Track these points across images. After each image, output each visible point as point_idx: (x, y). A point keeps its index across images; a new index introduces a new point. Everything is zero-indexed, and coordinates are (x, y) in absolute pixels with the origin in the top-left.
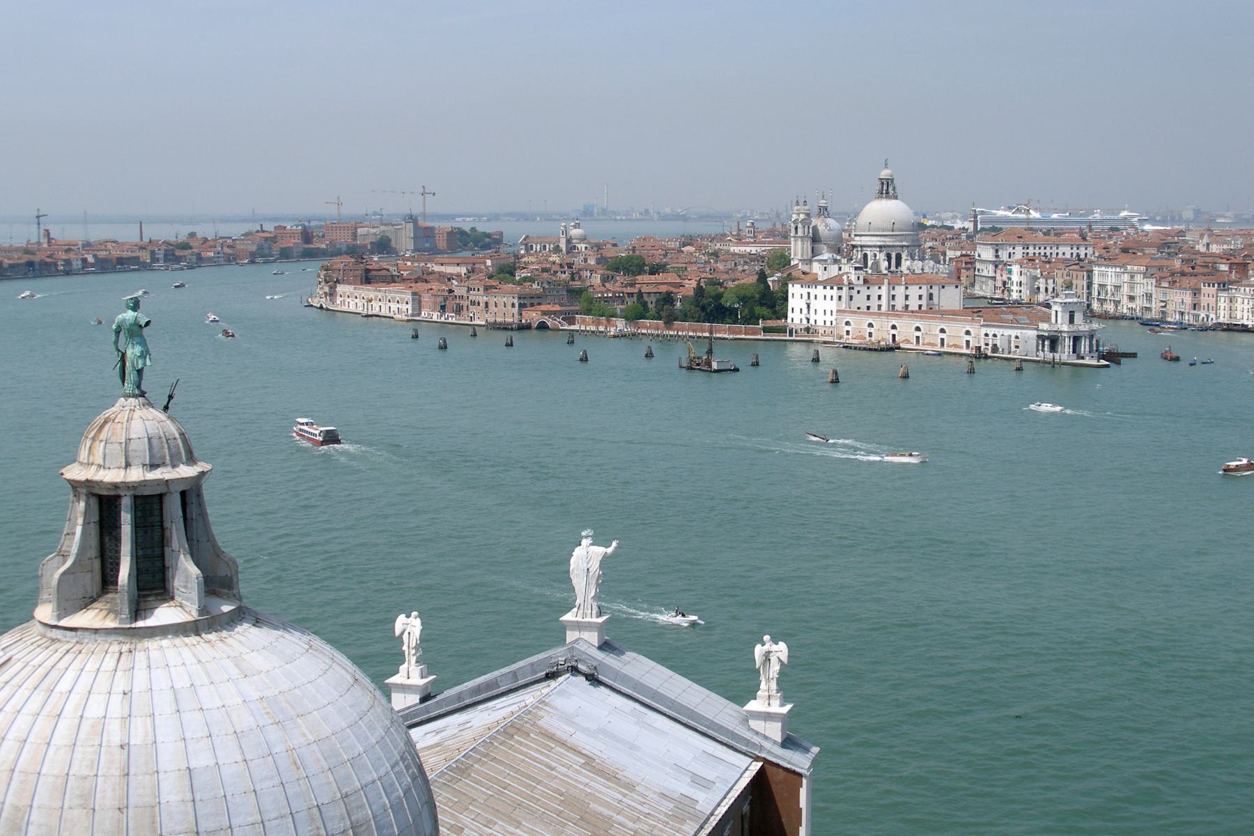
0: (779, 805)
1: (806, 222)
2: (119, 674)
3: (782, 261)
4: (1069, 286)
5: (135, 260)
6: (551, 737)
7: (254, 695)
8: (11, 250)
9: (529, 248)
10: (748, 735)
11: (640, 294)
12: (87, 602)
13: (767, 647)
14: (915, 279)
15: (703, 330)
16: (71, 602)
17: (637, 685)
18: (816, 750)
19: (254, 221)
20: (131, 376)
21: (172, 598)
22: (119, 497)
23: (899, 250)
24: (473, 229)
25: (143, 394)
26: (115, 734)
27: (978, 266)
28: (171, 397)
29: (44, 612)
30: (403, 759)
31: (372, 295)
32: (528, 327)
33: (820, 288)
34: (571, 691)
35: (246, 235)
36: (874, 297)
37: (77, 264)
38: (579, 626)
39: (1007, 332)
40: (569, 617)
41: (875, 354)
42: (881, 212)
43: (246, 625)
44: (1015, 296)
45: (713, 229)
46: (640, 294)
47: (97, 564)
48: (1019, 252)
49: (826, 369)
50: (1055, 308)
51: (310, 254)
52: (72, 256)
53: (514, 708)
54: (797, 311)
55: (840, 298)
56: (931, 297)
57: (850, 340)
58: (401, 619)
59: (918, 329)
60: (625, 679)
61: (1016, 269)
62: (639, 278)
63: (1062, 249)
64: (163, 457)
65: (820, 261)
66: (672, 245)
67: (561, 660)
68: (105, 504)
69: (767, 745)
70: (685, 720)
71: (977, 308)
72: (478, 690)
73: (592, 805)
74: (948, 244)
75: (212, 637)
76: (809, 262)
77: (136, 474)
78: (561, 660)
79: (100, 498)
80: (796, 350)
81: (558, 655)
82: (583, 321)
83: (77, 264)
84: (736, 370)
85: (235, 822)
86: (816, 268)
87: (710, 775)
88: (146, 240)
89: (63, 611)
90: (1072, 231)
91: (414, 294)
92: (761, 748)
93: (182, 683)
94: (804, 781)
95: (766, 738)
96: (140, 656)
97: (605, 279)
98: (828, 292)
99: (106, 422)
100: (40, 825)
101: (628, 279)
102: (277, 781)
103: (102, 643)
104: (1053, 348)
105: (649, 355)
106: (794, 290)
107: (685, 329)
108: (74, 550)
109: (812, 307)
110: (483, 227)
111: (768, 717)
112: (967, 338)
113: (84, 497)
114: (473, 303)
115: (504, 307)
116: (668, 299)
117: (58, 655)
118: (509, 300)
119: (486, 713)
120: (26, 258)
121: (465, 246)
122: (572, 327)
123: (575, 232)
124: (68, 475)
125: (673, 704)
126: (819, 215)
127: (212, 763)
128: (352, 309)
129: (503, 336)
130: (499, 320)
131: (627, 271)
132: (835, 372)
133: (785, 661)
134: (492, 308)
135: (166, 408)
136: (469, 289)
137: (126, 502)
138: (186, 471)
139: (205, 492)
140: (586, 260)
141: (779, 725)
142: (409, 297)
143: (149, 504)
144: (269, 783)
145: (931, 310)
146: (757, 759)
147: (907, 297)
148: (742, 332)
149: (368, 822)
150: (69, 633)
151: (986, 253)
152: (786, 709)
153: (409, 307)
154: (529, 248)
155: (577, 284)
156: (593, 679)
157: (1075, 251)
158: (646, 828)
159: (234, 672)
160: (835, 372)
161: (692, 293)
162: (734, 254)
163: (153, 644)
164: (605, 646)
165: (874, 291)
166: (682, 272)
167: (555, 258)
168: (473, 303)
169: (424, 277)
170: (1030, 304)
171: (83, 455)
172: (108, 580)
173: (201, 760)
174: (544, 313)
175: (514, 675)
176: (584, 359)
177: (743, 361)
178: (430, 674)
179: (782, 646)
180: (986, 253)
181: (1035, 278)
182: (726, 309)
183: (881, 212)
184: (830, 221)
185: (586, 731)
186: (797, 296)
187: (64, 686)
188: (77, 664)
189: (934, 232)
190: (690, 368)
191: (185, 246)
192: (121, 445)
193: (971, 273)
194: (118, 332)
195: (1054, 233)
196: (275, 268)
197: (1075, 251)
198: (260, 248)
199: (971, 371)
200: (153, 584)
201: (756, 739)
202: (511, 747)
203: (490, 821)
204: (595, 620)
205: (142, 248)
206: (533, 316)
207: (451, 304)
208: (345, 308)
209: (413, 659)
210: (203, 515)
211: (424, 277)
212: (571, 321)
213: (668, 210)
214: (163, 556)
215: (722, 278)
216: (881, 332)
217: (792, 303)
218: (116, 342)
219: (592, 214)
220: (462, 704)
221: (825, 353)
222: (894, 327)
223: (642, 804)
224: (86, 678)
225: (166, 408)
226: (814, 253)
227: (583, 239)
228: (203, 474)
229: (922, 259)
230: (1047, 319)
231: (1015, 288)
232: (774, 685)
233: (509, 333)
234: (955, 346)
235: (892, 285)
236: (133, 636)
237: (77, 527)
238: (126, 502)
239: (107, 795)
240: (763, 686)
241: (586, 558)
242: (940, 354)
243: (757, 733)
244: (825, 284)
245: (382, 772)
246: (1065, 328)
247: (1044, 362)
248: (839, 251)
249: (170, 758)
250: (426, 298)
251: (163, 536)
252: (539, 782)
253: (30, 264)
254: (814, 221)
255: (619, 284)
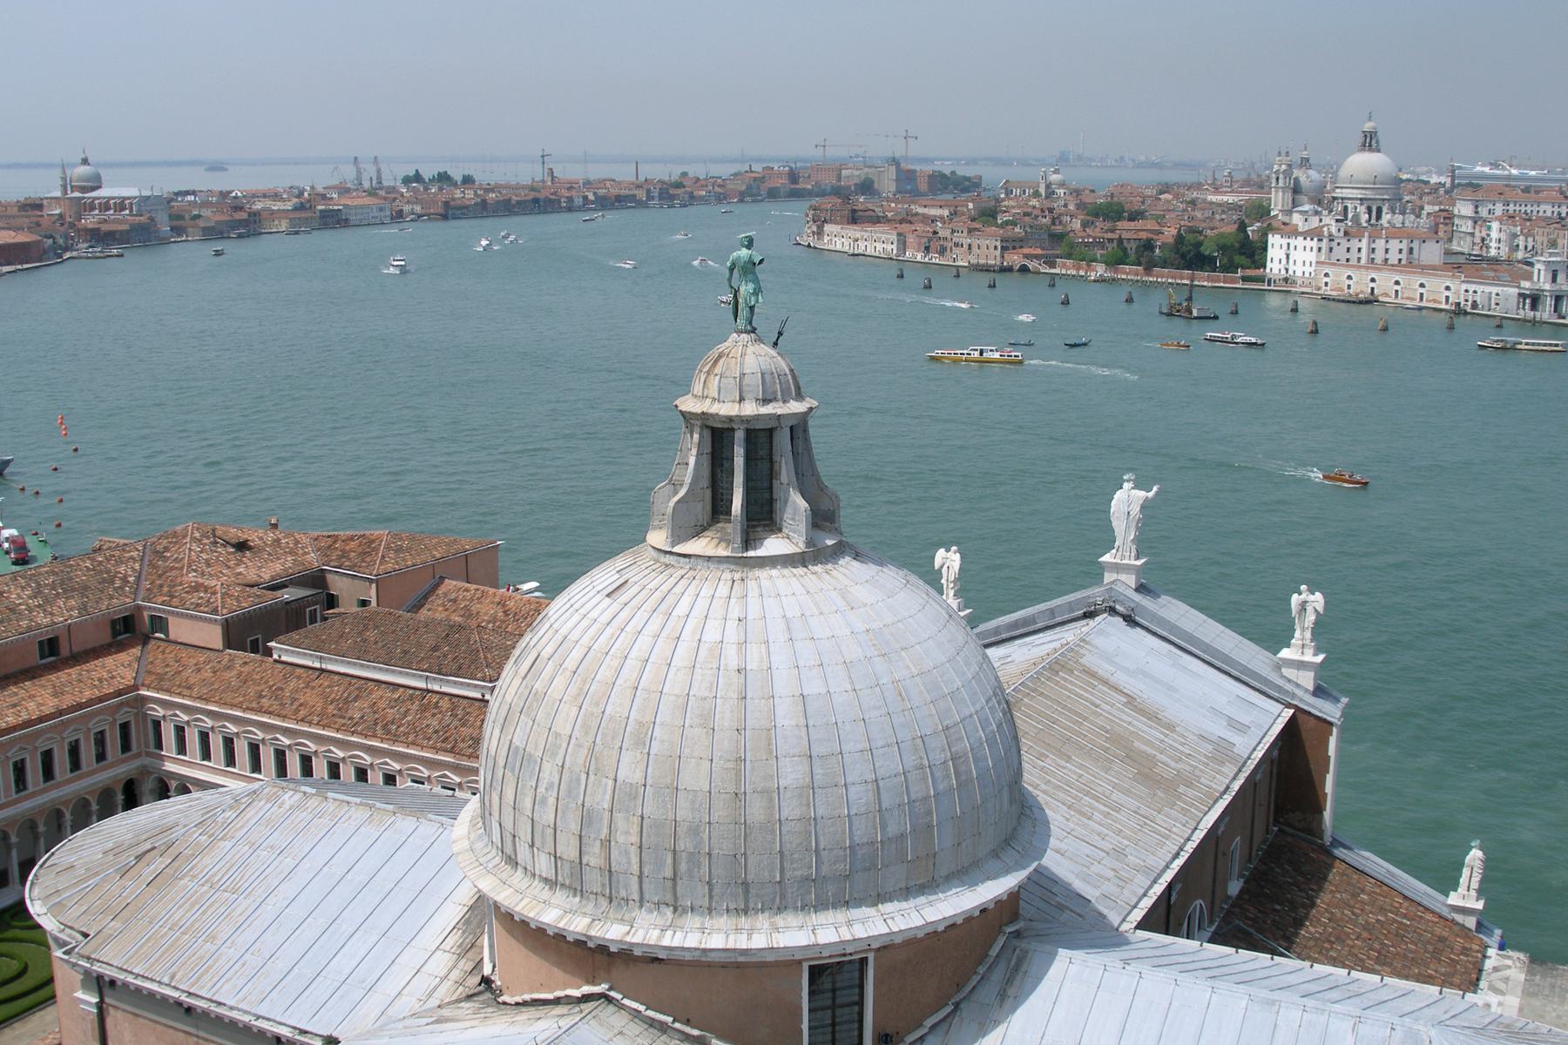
0: (1309, 751)
1: (1288, 173)
2: (733, 601)
3: (1262, 211)
4: (1553, 244)
5: (633, 198)
6: (1093, 675)
7: (861, 627)
8: (518, 187)
9: (1008, 193)
10: (1281, 682)
11: (1120, 240)
12: (698, 531)
13: (1303, 596)
14: (1394, 233)
15: (1184, 278)
16: (685, 529)
17: (1173, 628)
18: (1345, 700)
19: (743, 161)
20: (743, 313)
21: (780, 530)
22: (733, 430)
23: (1380, 203)
24: (953, 173)
25: (754, 331)
26: (731, 659)
27: (1456, 221)
28: (780, 334)
29: (658, 538)
30: (995, 695)
31: (858, 235)
32: (1009, 269)
33: (1300, 239)
34: (1108, 630)
35: (735, 175)
36: (1354, 250)
37: (578, 201)
38: (1117, 568)
39: (1488, 289)
40: (1107, 558)
41: (1354, 307)
42: (1361, 164)
43: (848, 559)
44: (1493, 252)
45: (1190, 178)
46: (1120, 240)
47: (708, 493)
48: (1499, 209)
49: (1305, 319)
50: (1538, 266)
51: (796, 194)
52: (574, 193)
53: (1057, 645)
54: (1276, 261)
55: (1320, 249)
56: (1411, 251)
57: (1328, 291)
58: (941, 553)
59: (1397, 283)
60: (1162, 621)
61: (1495, 225)
62: (1120, 224)
63: (1542, 208)
64: (775, 392)
65: (1301, 212)
66: (1148, 192)
67: (1099, 600)
68: (718, 435)
69: (1299, 692)
70: (1219, 664)
71: (1459, 264)
72: (1015, 625)
73: (1137, 744)
74: (1426, 198)
75: (818, 568)
76: (1289, 213)
77: (750, 409)
78: (1099, 600)
79: (713, 430)
80: (1274, 301)
81: (1095, 593)
82: (1064, 266)
83: (578, 201)
84: (1216, 318)
85: (846, 748)
86: (1297, 219)
87: (1246, 720)
88: (642, 179)
89: (677, 538)
90: (1551, 189)
91: (899, 234)
92: (1294, 696)
93: (793, 612)
94: (1335, 730)
95: (1298, 686)
96: (752, 584)
97: (1085, 225)
98: (1308, 243)
99: (720, 357)
100: (663, 741)
101: (1108, 225)
102: (884, 711)
103: (714, 572)
104: (1534, 307)
105: (1130, 300)
106: (1274, 241)
107: (1163, 276)
108: (688, 480)
109: (1291, 257)
110: (963, 171)
111: (1301, 665)
112: (1447, 293)
113: (697, 429)
114: (956, 245)
115: (986, 249)
116: (1148, 246)
117: (673, 580)
118: (992, 243)
119: (1025, 649)
120: (532, 195)
121: (945, 189)
122: (1057, 271)
123: (1054, 178)
124: (683, 408)
125: (1207, 648)
126: (1301, 166)
127: (824, 691)
128: (839, 247)
129: (986, 278)
130: (982, 262)
131: (1107, 217)
132: (1315, 323)
133: (1321, 609)
134: (975, 250)
135: (776, 344)
136: (953, 231)
137: (739, 435)
138: (796, 407)
139: (811, 431)
140: (1066, 206)
141: (1312, 674)
142: (894, 237)
143: (760, 437)
144: (877, 713)
145: (1410, 264)
146: (1289, 706)
147: (1387, 251)
148: (1220, 281)
149: (966, 754)
150: (682, 560)
151: (1464, 209)
152: (1320, 658)
153: (894, 247)
154: (1008, 193)
155: (1058, 229)
156: (1130, 620)
157: (1556, 209)
158: (1188, 768)
159: (840, 603)
160: (1315, 323)
161: (1171, 240)
162: (1211, 203)
163: (763, 574)
164: (1141, 588)
165: (1355, 244)
166: (1160, 219)
167: (1034, 202)
168: (956, 245)
169: (908, 219)
170: (1509, 261)
171: (697, 388)
172: (719, 509)
173: (813, 688)
174: (1026, 256)
175: (1052, 612)
176: (1066, 302)
177: (1223, 310)
178: (966, 607)
179: (1318, 596)
180: (1464, 209)
181: (1515, 236)
182: (1206, 257)
183: (1361, 164)
184: (1311, 172)
185: (1125, 670)
186: (1276, 246)
187: (681, 609)
188: (692, 590)
189: (1410, 186)
190: (1170, 315)
191: (679, 185)
192: (733, 379)
193: (1449, 228)
194: (732, 270)
195: (1530, 190)
196: (765, 206)
197: (1556, 209)
198: (749, 187)
199: (1451, 327)
200: (763, 516)
201: (1288, 687)
202: (1057, 683)
203: (1042, 755)
204: (1133, 562)
205: (639, 187)
206: (1015, 259)
207: (935, 245)
208: (832, 247)
209: (952, 593)
210: (808, 449)
211: (908, 219)
212: (1052, 265)
213: (1142, 158)
214: (771, 488)
215: (1201, 226)
216: (1360, 284)
217: (1271, 253)
218: (730, 280)
219: (1067, 160)
220: (998, 638)
221: (1303, 304)
222: (1373, 280)
223: (1183, 744)
224: (702, 604)
225: (776, 344)
226: (1295, 204)
227: (1062, 185)
228: (811, 409)
229: (1403, 213)
230: (1529, 277)
231: (1493, 244)
232: (1308, 635)
233: (992, 275)
234: (1434, 301)
235: (1372, 239)
236: (745, 565)
237: (690, 457)
238: (739, 435)
239: (726, 717)
240: (1297, 634)
241: (1127, 501)
242: (1420, 309)
243: (1289, 681)
244: (1305, 235)
245: (978, 707)
246: (1547, 287)
247: (1525, 321)
248: (1319, 203)
249: (784, 685)
250: (911, 239)
251: (772, 469)
252: (1085, 719)
253: (536, 201)
254: (1296, 173)
255: (1099, 230)
